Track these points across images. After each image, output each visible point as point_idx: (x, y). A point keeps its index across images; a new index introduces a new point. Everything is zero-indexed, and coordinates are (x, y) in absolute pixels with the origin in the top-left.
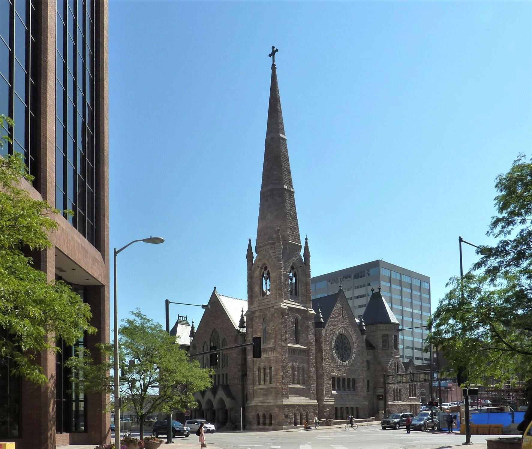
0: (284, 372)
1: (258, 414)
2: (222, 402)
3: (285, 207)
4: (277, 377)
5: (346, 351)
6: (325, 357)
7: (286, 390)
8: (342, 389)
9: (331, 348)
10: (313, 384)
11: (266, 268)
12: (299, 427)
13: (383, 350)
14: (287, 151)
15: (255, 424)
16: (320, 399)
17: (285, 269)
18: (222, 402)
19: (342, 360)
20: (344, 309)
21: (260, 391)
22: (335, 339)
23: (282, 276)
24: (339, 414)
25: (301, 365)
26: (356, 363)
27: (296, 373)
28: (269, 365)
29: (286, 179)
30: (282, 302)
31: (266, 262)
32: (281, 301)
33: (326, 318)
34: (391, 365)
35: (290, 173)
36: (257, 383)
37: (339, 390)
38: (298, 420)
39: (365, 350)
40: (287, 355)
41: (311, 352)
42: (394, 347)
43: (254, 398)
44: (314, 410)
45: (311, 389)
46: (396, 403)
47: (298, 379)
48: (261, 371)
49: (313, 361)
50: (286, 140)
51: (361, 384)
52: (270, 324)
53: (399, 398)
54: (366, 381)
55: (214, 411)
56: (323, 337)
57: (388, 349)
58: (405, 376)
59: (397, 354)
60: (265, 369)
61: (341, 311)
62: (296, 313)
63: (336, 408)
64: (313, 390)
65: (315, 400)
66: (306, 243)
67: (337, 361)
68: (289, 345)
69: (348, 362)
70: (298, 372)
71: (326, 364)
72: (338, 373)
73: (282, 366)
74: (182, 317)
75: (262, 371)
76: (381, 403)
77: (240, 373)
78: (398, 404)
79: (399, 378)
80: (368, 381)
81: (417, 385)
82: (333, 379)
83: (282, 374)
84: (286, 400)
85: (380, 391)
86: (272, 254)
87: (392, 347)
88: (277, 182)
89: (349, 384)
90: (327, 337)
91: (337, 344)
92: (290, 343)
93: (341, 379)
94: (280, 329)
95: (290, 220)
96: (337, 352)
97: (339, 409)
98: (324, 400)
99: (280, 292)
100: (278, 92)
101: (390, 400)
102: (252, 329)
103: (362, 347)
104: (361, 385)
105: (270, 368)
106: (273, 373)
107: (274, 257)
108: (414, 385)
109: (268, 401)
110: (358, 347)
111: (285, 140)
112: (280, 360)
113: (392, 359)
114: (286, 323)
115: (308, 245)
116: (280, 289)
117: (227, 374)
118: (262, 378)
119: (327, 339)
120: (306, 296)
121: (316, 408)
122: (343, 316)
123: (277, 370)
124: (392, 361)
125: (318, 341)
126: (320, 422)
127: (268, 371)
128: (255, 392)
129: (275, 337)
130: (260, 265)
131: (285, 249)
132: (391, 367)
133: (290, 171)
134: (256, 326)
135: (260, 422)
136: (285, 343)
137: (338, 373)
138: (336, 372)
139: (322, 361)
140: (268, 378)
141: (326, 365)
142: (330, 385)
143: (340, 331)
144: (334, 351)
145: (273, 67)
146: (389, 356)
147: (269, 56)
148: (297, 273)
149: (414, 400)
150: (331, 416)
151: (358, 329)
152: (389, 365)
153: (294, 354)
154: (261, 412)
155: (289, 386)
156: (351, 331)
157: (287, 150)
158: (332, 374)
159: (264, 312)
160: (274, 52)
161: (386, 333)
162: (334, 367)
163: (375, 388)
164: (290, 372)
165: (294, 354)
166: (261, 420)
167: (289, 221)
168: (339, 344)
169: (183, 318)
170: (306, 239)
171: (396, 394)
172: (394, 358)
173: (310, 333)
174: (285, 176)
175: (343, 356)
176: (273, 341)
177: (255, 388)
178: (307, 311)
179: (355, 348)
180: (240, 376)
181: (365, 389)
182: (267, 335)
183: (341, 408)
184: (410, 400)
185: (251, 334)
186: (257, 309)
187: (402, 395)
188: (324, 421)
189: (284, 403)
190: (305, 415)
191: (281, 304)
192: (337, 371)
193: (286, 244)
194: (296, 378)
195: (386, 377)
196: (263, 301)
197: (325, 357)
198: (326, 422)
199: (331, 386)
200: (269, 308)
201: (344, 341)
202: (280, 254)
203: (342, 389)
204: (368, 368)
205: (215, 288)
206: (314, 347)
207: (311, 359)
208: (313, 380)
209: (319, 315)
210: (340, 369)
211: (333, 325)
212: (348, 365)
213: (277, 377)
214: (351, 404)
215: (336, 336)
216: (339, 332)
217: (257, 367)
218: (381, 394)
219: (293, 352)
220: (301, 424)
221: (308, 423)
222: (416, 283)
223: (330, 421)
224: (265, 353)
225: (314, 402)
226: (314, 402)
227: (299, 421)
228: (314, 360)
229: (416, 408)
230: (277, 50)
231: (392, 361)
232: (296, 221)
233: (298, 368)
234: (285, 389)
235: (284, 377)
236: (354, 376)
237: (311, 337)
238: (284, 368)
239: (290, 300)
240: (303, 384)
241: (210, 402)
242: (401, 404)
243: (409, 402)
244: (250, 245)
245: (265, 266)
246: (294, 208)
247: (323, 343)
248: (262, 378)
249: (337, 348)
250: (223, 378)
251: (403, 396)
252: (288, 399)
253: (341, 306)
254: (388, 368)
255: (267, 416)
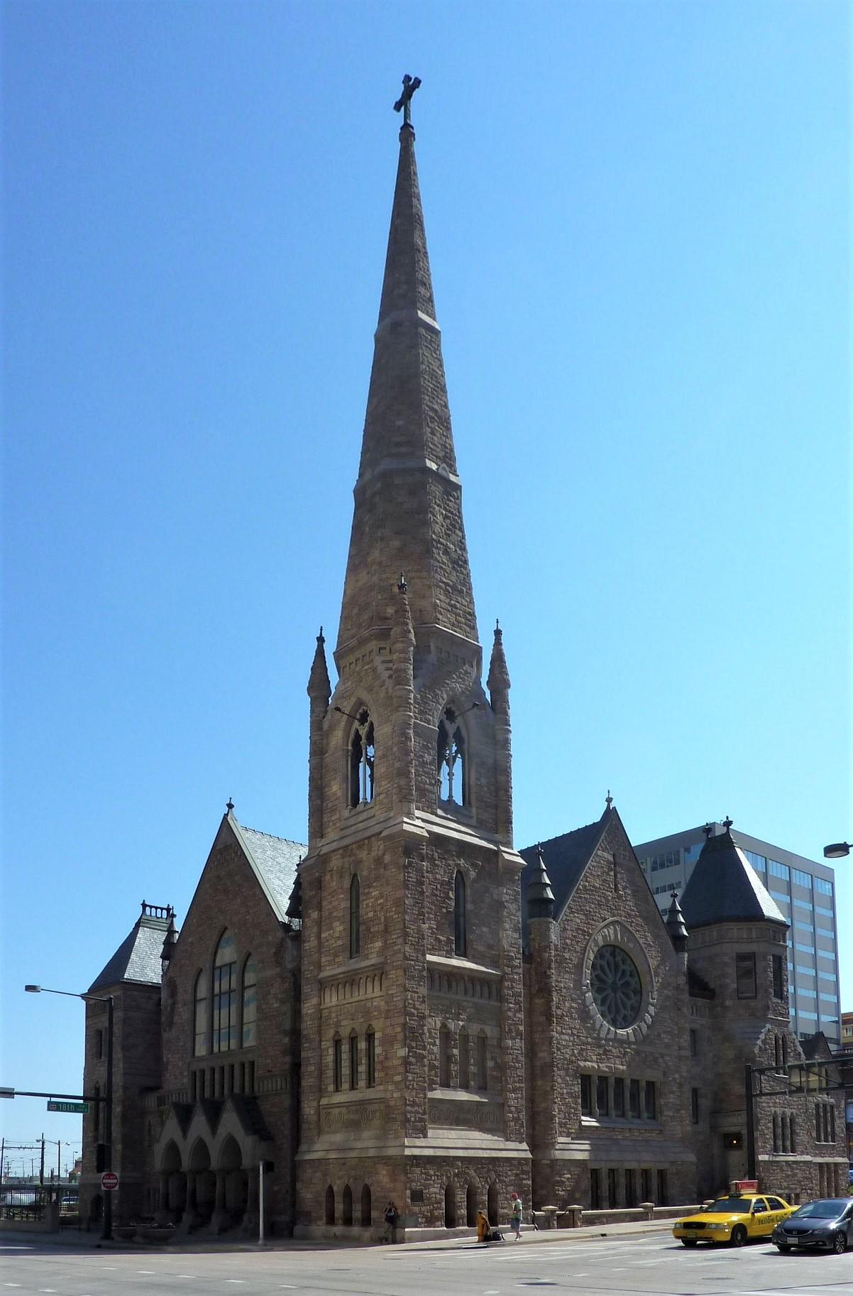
0: (410, 1048)
1: (331, 1188)
2: (232, 1146)
3: (426, 524)
4: (389, 1064)
5: (629, 998)
6: (559, 1012)
7: (419, 1106)
8: (613, 1113)
9: (578, 983)
10: (514, 1090)
11: (364, 718)
12: (462, 1232)
13: (739, 998)
14: (441, 366)
15: (321, 1219)
16: (538, 1142)
17: (421, 712)
18: (232, 1146)
19: (614, 1023)
20: (618, 869)
21: (337, 1111)
22: (592, 956)
23: (411, 732)
24: (605, 1190)
25: (474, 1029)
26: (659, 1035)
27: (456, 1051)
28: (365, 1026)
29: (435, 445)
30: (410, 815)
31: (365, 696)
32: (405, 810)
33: (563, 888)
34: (764, 1042)
35: (448, 429)
36: (331, 1088)
37: (604, 1115)
38: (460, 1208)
39: (686, 997)
40: (423, 990)
41: (508, 988)
42: (772, 991)
43: (319, 1134)
44: (517, 1175)
45: (510, 1106)
46: (782, 1158)
47: (464, 1073)
48: (343, 1047)
49: (515, 1015)
50: (440, 332)
51: (672, 1099)
52: (371, 890)
53: (788, 1143)
54: (688, 1095)
55: (213, 1174)
56: (553, 947)
57: (755, 997)
58: (816, 1070)
59: (783, 1011)
60: (353, 1040)
61: (612, 873)
62: (459, 857)
63: (595, 1173)
64: (513, 1109)
65: (520, 1142)
66: (498, 643)
67: (598, 1026)
68: (430, 958)
69: (634, 1030)
70: (465, 1052)
71: (563, 1034)
72: (600, 1061)
73: (404, 1025)
74: (156, 908)
75: (345, 1048)
76: (737, 1158)
77: (288, 1059)
78: (787, 1162)
79: (796, 1079)
80: (695, 1092)
81: (839, 1107)
82: (586, 1079)
83: (402, 1052)
84: (418, 1142)
85: (735, 1123)
86: (381, 668)
87: (766, 991)
88: (403, 450)
89: (634, 1097)
90: (565, 947)
91: (599, 972)
92: (433, 951)
93: (612, 1081)
94: (399, 903)
95: (444, 564)
96: (599, 997)
97: (604, 1175)
98: (553, 1144)
99: (403, 782)
100: (419, 200)
101: (763, 1147)
102: (320, 910)
103: (677, 988)
104: (673, 1101)
105: (370, 1037)
106: (378, 1050)
107: (387, 674)
108: (829, 1108)
109: (359, 1145)
110: (664, 986)
111: (436, 333)
112: (400, 1005)
113: (768, 1026)
114: (422, 883)
115: (501, 650)
116: (404, 773)
117: (252, 1064)
118: (346, 1071)
119: (567, 955)
120: (496, 807)
121: (525, 1168)
122: (616, 889)
123: (389, 1041)
124: (769, 1031)
125: (534, 957)
126: (539, 1217)
127: (362, 1045)
128: (323, 1112)
129: (386, 931)
130: (347, 706)
131: (422, 650)
132: (766, 1049)
133: (449, 423)
134: (331, 902)
135: (337, 1215)
136: (417, 951)
137: (600, 1061)
138: (594, 1058)
139: (550, 1022)
140: (362, 1068)
141: (564, 1038)
142: (576, 1097)
143: (606, 933)
144: (589, 995)
145: (407, 133)
146: (759, 1016)
147: (395, 108)
148: (464, 733)
149: (832, 1151)
150: (577, 1195)
151: (664, 933)
152: (759, 1042)
153: (450, 986)
154: (338, 1182)
155: (430, 1095)
156: (644, 937)
157: (440, 360)
158: (582, 1064)
159: (355, 855)
160: (411, 86)
161: (746, 948)
162: (588, 1044)
163: (716, 1112)
164: (436, 1049)
165: (450, 986)
166: (339, 1208)
167: (441, 568)
168: (606, 975)
169: (159, 910)
170: (498, 633)
171: (779, 1131)
172: (773, 1021)
173: (507, 926)
174: (432, 433)
175: (618, 1012)
176: (379, 944)
177: (324, 1101)
178: (497, 854)
179: (656, 988)
180: (287, 1067)
181: (686, 1114)
182: (362, 928)
183: (612, 1172)
184: (820, 1151)
185: (315, 930)
186: (335, 845)
187: (798, 1134)
188: (553, 1211)
189: (408, 1152)
190: (485, 1191)
191: (405, 819)
192: (599, 1054)
193: (426, 631)
194: (454, 1068)
195: (749, 1074)
196: (352, 822)
197: (559, 1012)
198: (559, 1216)
199: (580, 1101)
200: (368, 838)
201: (622, 967)
202: (406, 660)
203: (613, 1113)
204: (695, 1053)
205: (230, 806)
206: (520, 971)
207: (510, 1009)
208: (517, 1079)
209: (540, 876)
210: (605, 1051)
211: (584, 914)
212: (632, 1039)
213: (389, 1064)
214: (646, 1160)
215: (596, 949)
216: (604, 937)
217: (331, 1033)
218: (734, 1129)
219: (445, 983)
220: (471, 1223)
221: (493, 1220)
222: (801, 880)
223: (572, 1211)
224: (355, 987)
225: (519, 1150)
226: (519, 1150)
227: (464, 1212)
228: (521, 1016)
229: (836, 1172)
230: (418, 82)
231: (767, 1032)
232: (464, 572)
233: (465, 1038)
234: (414, 1104)
235: (410, 1064)
236: (650, 1075)
237: (510, 938)
238: (412, 1035)
239: (440, 812)
240: (482, 1089)
241: (201, 1149)
242: (794, 1162)
243: (815, 1155)
244: (320, 653)
245: (361, 711)
246: (460, 534)
247: (553, 965)
248: (346, 1071)
249: (599, 985)
250: (243, 1074)
251: (802, 1137)
252: (425, 1136)
253: (611, 859)
254: (756, 1051)
255: (357, 1192)
